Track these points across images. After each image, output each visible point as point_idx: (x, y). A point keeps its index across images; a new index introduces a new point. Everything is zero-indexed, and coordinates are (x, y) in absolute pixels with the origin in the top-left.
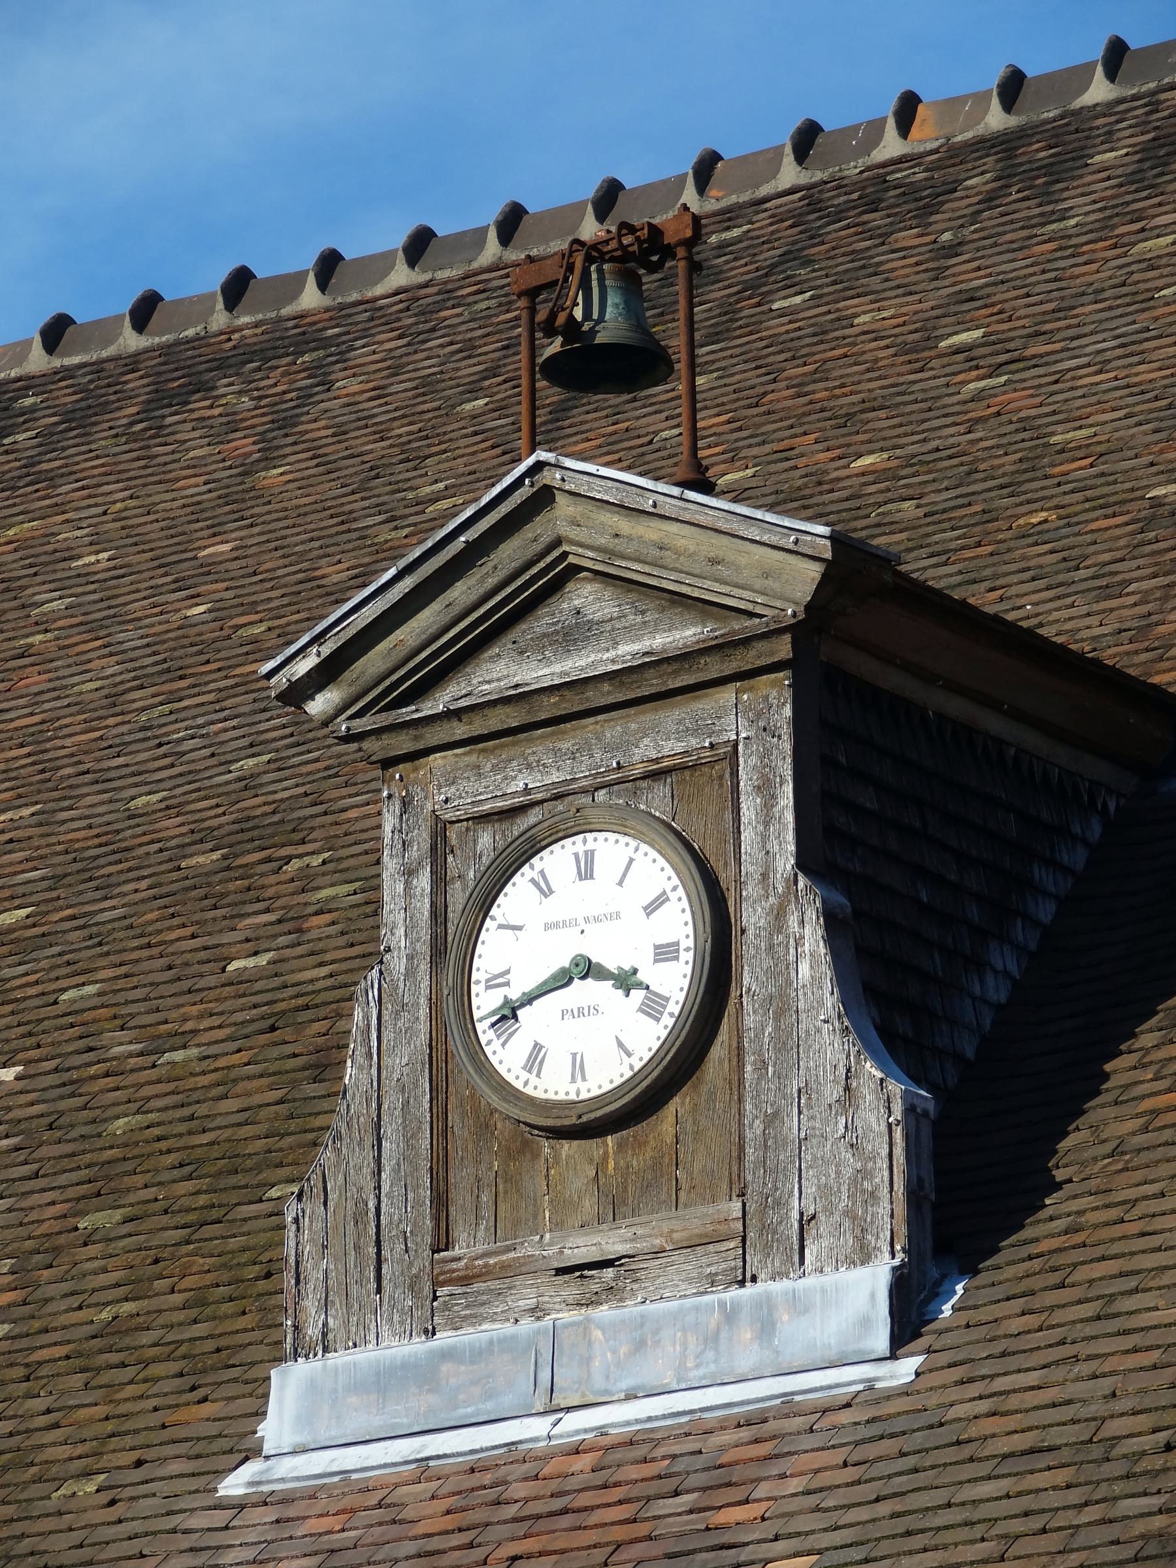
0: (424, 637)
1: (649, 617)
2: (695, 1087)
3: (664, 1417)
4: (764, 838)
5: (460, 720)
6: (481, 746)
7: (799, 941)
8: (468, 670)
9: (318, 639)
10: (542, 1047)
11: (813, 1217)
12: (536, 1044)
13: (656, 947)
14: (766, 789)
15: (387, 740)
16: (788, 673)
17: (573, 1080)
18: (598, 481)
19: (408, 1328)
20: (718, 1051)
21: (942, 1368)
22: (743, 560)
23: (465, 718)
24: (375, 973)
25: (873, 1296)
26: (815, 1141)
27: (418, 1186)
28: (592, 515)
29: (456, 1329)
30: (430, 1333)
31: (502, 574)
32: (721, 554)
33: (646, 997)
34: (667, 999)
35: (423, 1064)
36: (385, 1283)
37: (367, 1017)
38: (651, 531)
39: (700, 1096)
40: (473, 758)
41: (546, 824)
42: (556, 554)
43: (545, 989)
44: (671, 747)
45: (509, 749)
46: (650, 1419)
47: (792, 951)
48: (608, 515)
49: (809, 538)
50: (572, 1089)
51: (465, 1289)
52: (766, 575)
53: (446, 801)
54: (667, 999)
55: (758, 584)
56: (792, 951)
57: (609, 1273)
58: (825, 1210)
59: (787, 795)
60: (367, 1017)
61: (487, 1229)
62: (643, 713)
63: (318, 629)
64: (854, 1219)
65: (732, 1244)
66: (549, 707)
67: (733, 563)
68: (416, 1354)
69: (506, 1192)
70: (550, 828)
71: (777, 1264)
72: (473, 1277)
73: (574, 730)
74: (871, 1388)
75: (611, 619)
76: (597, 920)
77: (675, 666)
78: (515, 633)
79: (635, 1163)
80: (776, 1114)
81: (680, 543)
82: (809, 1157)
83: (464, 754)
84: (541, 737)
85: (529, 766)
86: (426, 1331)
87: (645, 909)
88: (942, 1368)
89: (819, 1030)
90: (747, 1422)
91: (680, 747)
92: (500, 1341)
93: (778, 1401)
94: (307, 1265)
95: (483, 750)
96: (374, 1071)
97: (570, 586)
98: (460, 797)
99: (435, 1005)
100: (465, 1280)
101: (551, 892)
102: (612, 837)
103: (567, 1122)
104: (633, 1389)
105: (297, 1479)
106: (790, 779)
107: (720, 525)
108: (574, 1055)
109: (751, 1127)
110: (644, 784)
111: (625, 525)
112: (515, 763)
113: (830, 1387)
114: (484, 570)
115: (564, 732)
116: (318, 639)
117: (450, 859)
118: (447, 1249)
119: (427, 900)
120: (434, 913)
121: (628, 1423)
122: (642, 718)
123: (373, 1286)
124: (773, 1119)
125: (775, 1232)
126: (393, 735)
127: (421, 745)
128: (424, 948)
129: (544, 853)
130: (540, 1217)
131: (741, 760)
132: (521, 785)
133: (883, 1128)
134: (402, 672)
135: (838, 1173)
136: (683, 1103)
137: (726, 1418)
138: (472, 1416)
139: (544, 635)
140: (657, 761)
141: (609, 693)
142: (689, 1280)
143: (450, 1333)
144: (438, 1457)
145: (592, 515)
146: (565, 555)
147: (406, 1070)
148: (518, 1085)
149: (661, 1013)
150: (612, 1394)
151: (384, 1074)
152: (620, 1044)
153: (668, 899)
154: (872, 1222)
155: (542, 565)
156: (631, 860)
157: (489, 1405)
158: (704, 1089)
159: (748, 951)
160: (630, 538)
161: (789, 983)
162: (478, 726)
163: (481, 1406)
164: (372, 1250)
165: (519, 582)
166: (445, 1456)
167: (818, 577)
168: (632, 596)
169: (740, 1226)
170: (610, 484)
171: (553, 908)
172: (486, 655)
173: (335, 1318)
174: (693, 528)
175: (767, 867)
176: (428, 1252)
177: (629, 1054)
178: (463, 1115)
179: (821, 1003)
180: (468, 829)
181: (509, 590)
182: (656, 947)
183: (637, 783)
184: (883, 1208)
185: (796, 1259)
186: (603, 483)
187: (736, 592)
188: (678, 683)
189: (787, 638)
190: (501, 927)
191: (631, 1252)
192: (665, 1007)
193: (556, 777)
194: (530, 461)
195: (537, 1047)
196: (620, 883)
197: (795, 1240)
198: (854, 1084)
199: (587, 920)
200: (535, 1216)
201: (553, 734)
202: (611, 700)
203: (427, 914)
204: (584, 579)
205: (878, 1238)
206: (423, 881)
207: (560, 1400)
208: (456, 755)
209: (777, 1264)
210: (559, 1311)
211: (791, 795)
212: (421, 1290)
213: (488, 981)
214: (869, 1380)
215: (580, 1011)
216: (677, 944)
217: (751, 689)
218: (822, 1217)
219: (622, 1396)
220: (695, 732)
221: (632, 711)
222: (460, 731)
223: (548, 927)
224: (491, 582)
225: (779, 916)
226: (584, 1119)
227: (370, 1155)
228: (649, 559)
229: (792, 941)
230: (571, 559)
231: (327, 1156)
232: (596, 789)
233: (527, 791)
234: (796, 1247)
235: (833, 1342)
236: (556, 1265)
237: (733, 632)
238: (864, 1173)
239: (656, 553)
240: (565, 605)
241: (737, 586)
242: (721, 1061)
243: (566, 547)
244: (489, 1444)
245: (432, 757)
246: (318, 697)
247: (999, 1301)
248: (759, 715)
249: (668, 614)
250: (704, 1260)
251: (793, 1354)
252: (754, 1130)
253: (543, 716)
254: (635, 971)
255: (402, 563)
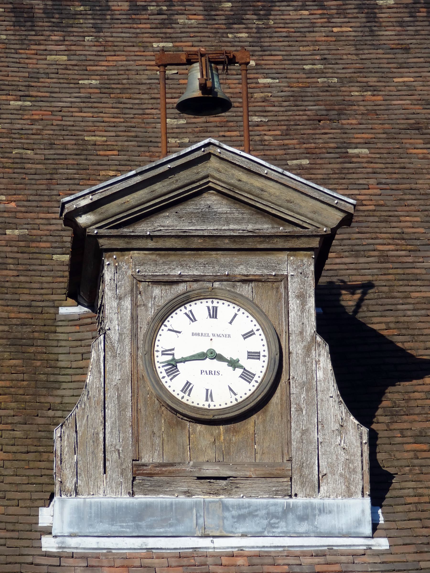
0: (139, 202)
1: (245, 216)
2: (264, 412)
3: (271, 547)
4: (301, 317)
5: (152, 240)
6: (157, 252)
7: (317, 362)
8: (152, 219)
9: (92, 193)
10: (190, 384)
11: (325, 475)
12: (188, 382)
13: (248, 352)
14: (302, 297)
15: (113, 241)
16: (313, 253)
17: (207, 400)
18: (237, 157)
19: (120, 491)
20: (275, 399)
21: (400, 545)
22: (303, 204)
23: (154, 239)
24: (102, 337)
25: (363, 511)
26: (325, 444)
27: (126, 432)
28: (228, 170)
29: (146, 495)
30: (133, 494)
31: (180, 184)
32: (292, 199)
33: (243, 372)
34: (254, 375)
35: (128, 381)
36: (107, 470)
37: (98, 356)
38: (258, 182)
39: (266, 416)
40: (154, 257)
41: (196, 292)
42: (205, 181)
43: (193, 358)
44: (254, 271)
45: (173, 257)
46: (264, 547)
47: (314, 366)
48: (237, 171)
49: (343, 203)
50: (206, 404)
51: (149, 478)
52: (314, 212)
53: (139, 272)
54: (254, 375)
55: (310, 215)
56: (314, 366)
57: (224, 482)
58: (330, 472)
59: (311, 302)
60: (98, 356)
61: (159, 455)
62: (241, 255)
63: (94, 188)
64: (346, 478)
65: (285, 480)
66: (197, 243)
67: (298, 204)
68: (133, 503)
69: (168, 441)
70: (198, 294)
71: (308, 490)
72: (154, 474)
73: (206, 255)
74: (370, 549)
75: (226, 213)
76: (218, 336)
77: (262, 239)
78: (178, 208)
79: (234, 439)
80: (307, 430)
81: (272, 191)
82: (323, 450)
83: (149, 254)
84: (189, 255)
85: (181, 265)
86: (129, 493)
87: (243, 336)
88: (400, 545)
89: (328, 400)
90: (317, 555)
91: (259, 272)
92: (176, 504)
93: (326, 548)
94: (66, 457)
95: (159, 254)
96: (102, 379)
97: (205, 195)
98: (146, 272)
99: (134, 358)
100: (151, 475)
101: (196, 320)
102: (226, 303)
103: (207, 417)
104: (245, 532)
105: (84, 549)
106: (313, 296)
107: (299, 188)
108: (207, 390)
109: (294, 434)
110: (238, 284)
111: (244, 177)
112: (174, 263)
113: (350, 546)
114: (171, 180)
115: (200, 255)
116: (92, 193)
117: (139, 296)
118: (138, 460)
119: (129, 311)
120: (132, 318)
121: (253, 547)
122: (240, 257)
123: (102, 470)
124: (304, 432)
125: (307, 478)
126: (117, 239)
127: (130, 246)
128: (127, 332)
129: (192, 303)
130: (186, 454)
131: (289, 284)
132: (179, 273)
133: (359, 445)
134: (125, 214)
135: (337, 458)
136: (258, 418)
137: (302, 552)
138: (163, 532)
139: (192, 213)
140: (247, 276)
141: (227, 243)
142: (265, 492)
143: (143, 496)
144: (158, 549)
145: (228, 170)
146: (209, 182)
147: (119, 382)
148: (179, 397)
149: (251, 380)
150: (236, 534)
151: (107, 381)
152: (230, 389)
153: (254, 334)
154: (353, 481)
155: (198, 184)
156: (236, 315)
157: (172, 529)
158: (269, 414)
159: (293, 362)
160: (246, 183)
161: (312, 378)
162: (160, 244)
163: (168, 530)
164: (101, 455)
165: (186, 189)
166: (161, 549)
167: (340, 219)
168: (237, 206)
169: (290, 473)
170: (244, 159)
171: (195, 327)
172: (162, 215)
173: (81, 481)
174: (281, 186)
175: (303, 329)
176: (130, 460)
177: (235, 394)
178: (146, 404)
179: (328, 389)
180: (148, 285)
181: (181, 191)
182: (248, 352)
183: (235, 283)
184: (359, 476)
185: (317, 490)
186: (240, 158)
187: (298, 216)
188: (262, 246)
189: (318, 239)
190: (169, 330)
191: (234, 476)
192: (253, 378)
193: (196, 273)
194: (206, 141)
195: (188, 384)
196: (231, 323)
197: (316, 483)
198: (345, 425)
199: (214, 335)
200: (184, 453)
201: (195, 254)
202: (228, 246)
203: (129, 318)
204: (212, 193)
205: (356, 488)
206: (127, 303)
207: (208, 532)
208: (145, 254)
209: (308, 490)
210: (198, 495)
211: (314, 302)
212: (127, 475)
213: (162, 351)
214: (368, 545)
215: (210, 372)
216: (259, 353)
217: (294, 256)
218: (329, 475)
219: (240, 535)
220: (266, 268)
221: (236, 253)
222: (151, 244)
223: (193, 334)
224: (174, 186)
225: (308, 350)
226: (216, 417)
227: (101, 414)
228: (255, 194)
229: (314, 362)
230: (210, 184)
231: (77, 411)
232: (215, 281)
233: (180, 276)
234: (317, 486)
235: (344, 527)
236: (197, 475)
237: (295, 232)
238: (348, 461)
239: (258, 192)
240: (202, 202)
241: (298, 214)
242: (277, 404)
243: (210, 179)
244: (184, 547)
245: (131, 252)
246: (83, 216)
247: (405, 520)
248: (298, 267)
249: (255, 216)
250: (271, 484)
251: (323, 528)
252: (296, 435)
253: (194, 246)
254: (239, 361)
255: (139, 170)
